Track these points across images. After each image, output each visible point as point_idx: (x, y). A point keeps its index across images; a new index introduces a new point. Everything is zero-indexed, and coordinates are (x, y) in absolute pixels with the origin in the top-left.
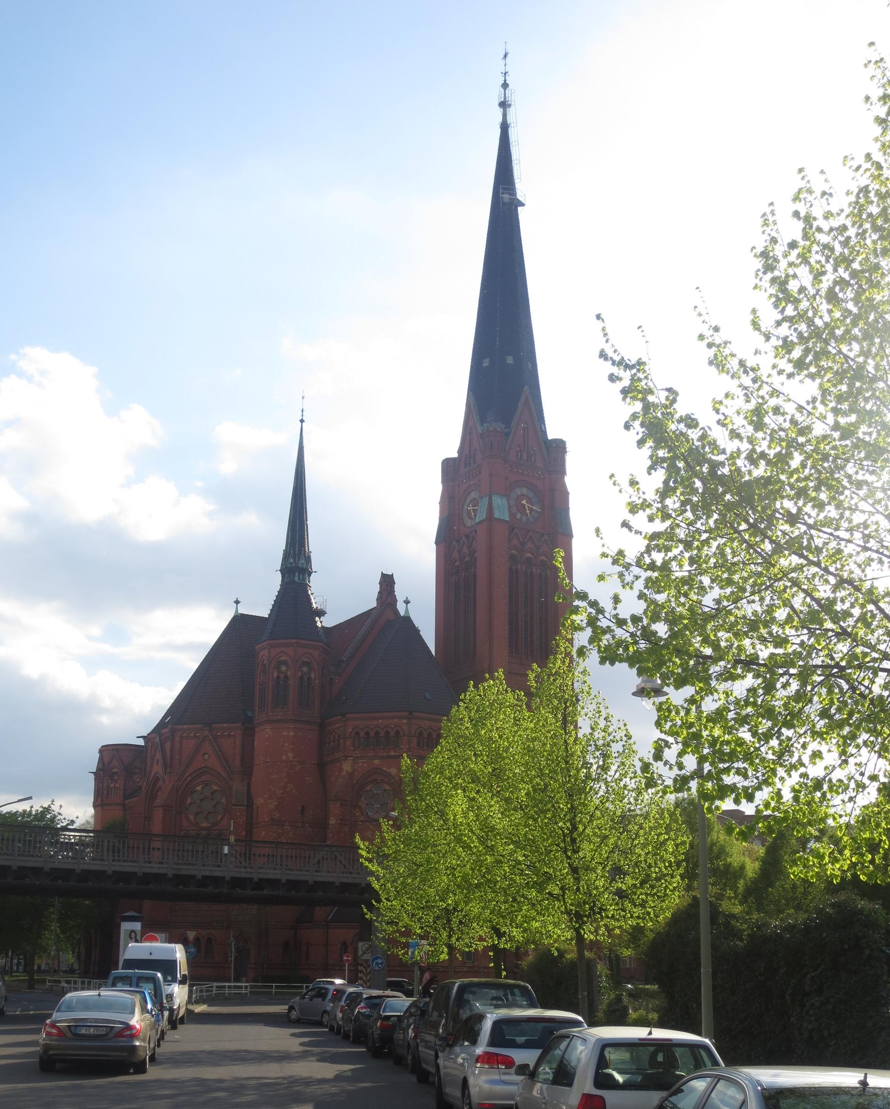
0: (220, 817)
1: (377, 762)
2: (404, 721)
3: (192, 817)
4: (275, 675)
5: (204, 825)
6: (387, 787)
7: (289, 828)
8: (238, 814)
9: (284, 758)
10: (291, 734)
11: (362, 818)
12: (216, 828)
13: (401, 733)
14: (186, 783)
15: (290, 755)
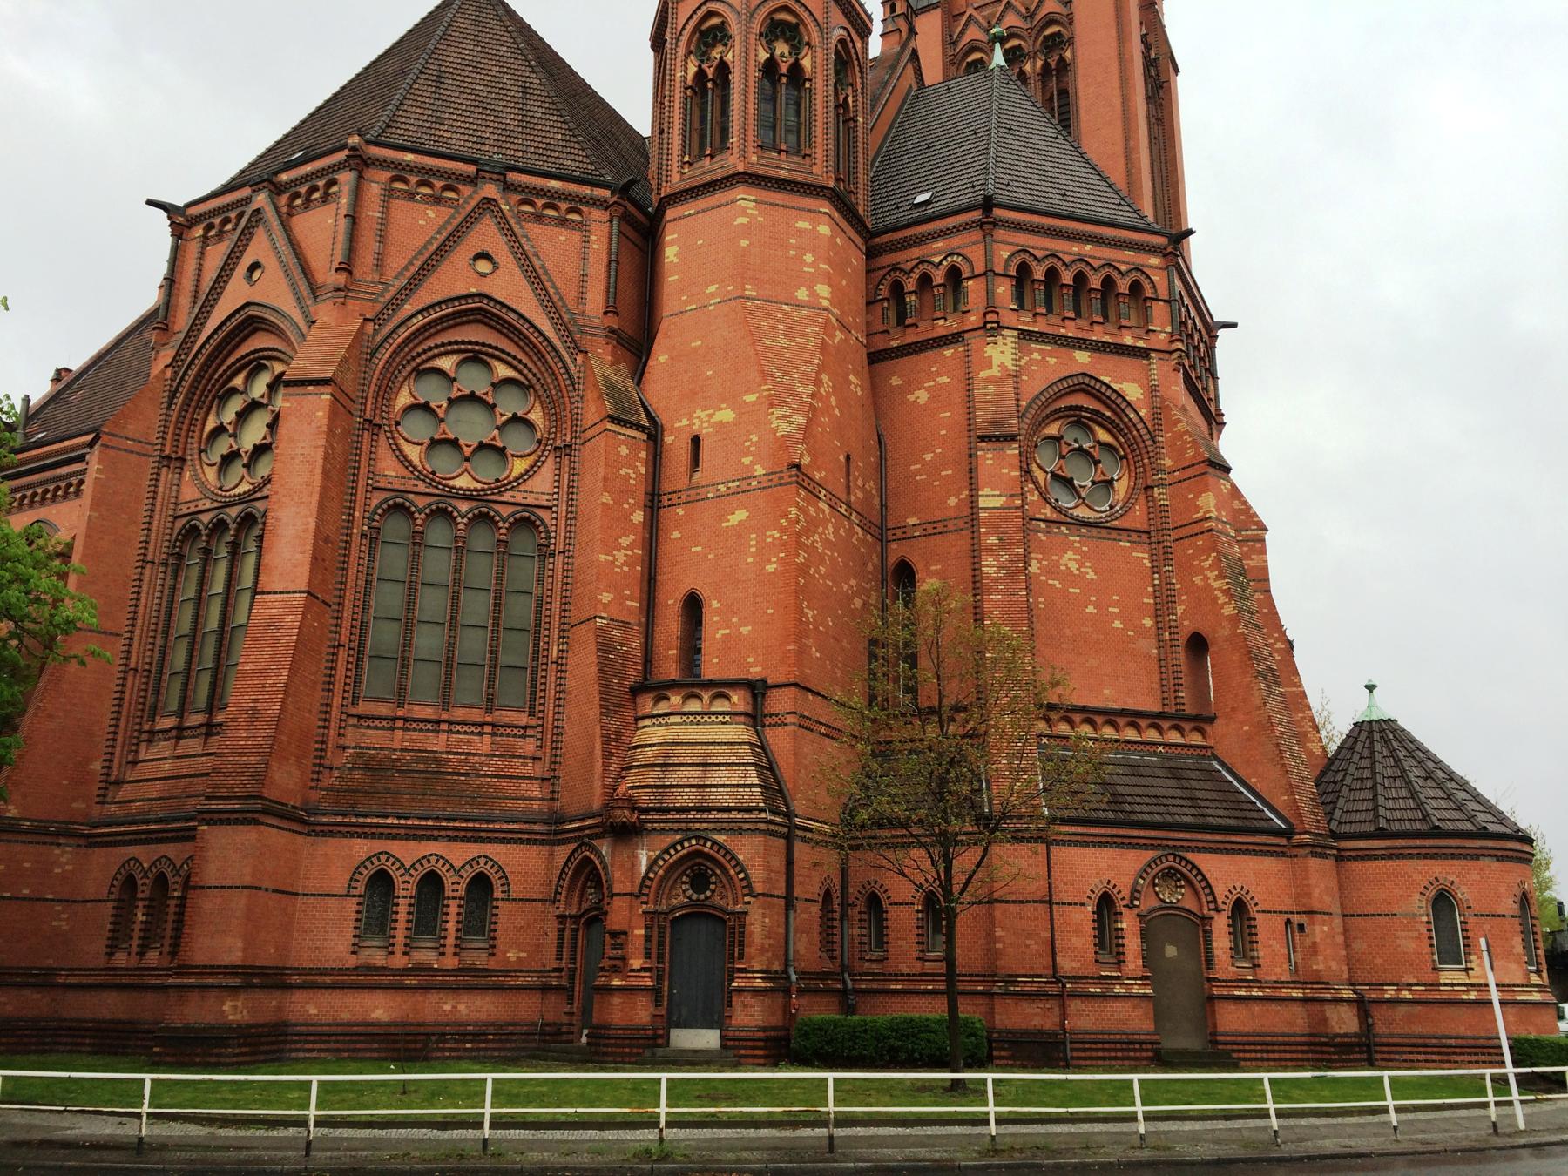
0: (519, 466)
1: (1082, 357)
2: (1155, 261)
3: (413, 453)
4: (764, 56)
5: (463, 482)
6: (1104, 436)
7: (826, 508)
8: (624, 450)
9: (802, 294)
10: (824, 230)
11: (1047, 512)
12: (507, 497)
13: (1149, 293)
14: (404, 333)
15: (823, 290)
